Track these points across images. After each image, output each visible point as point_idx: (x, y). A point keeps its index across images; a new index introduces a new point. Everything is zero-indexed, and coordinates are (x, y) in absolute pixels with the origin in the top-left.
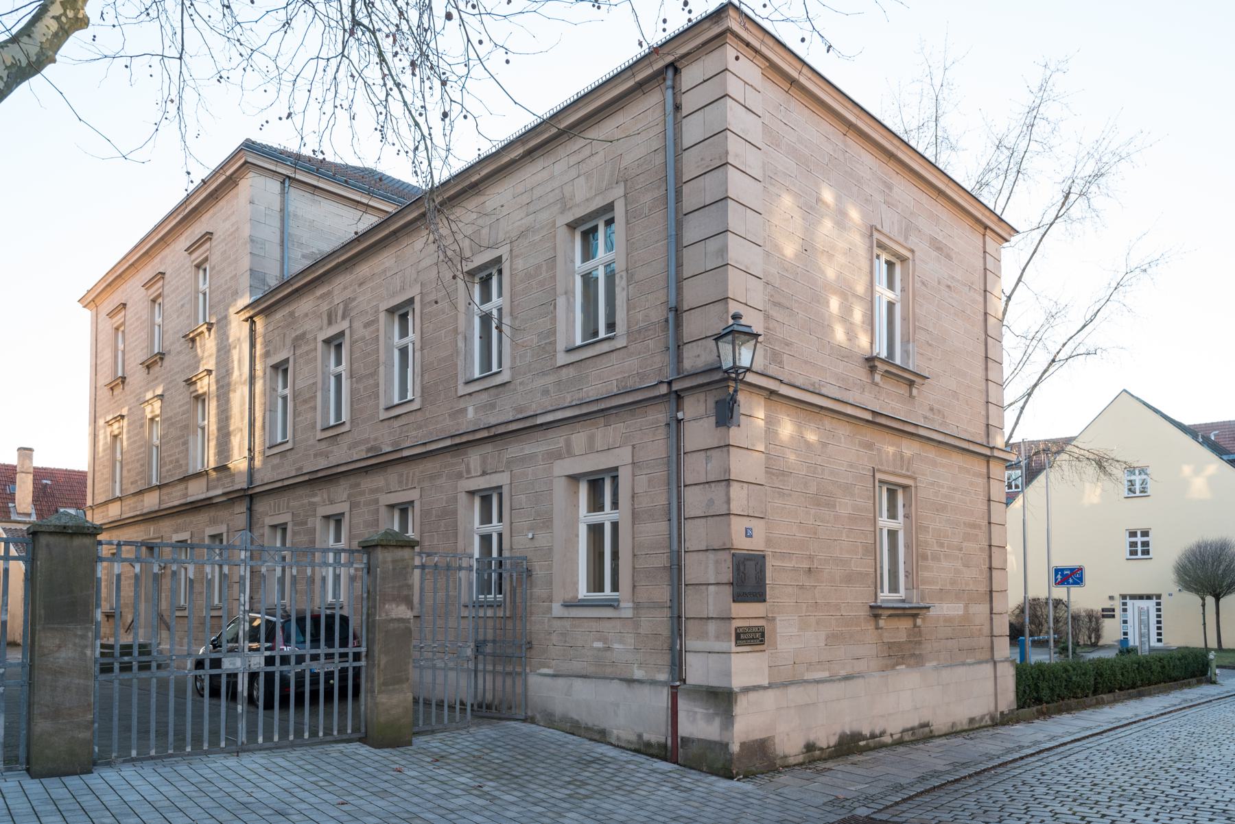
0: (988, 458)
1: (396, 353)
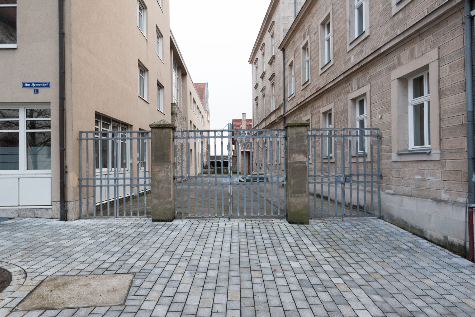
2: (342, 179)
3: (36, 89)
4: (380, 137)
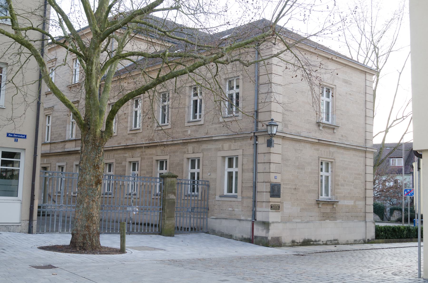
0: (365, 152)
2: (190, 210)
3: (16, 138)
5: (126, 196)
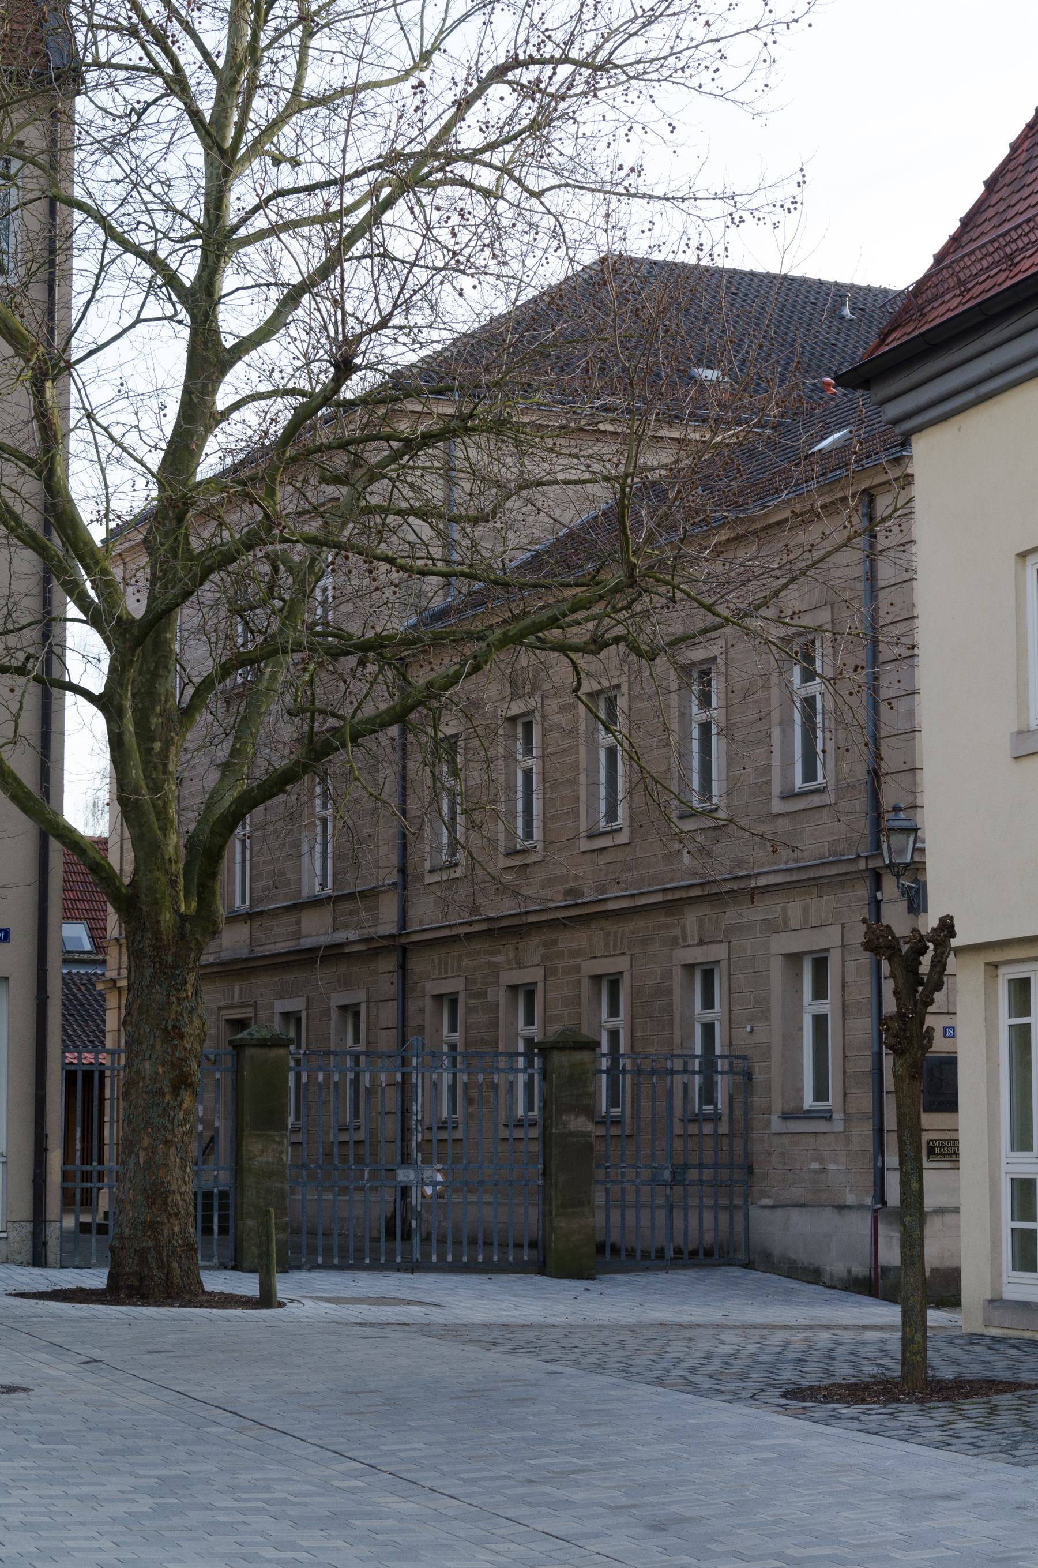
1: (603, 755)
2: (667, 1175)
4: (749, 1076)
5: (504, 1133)
